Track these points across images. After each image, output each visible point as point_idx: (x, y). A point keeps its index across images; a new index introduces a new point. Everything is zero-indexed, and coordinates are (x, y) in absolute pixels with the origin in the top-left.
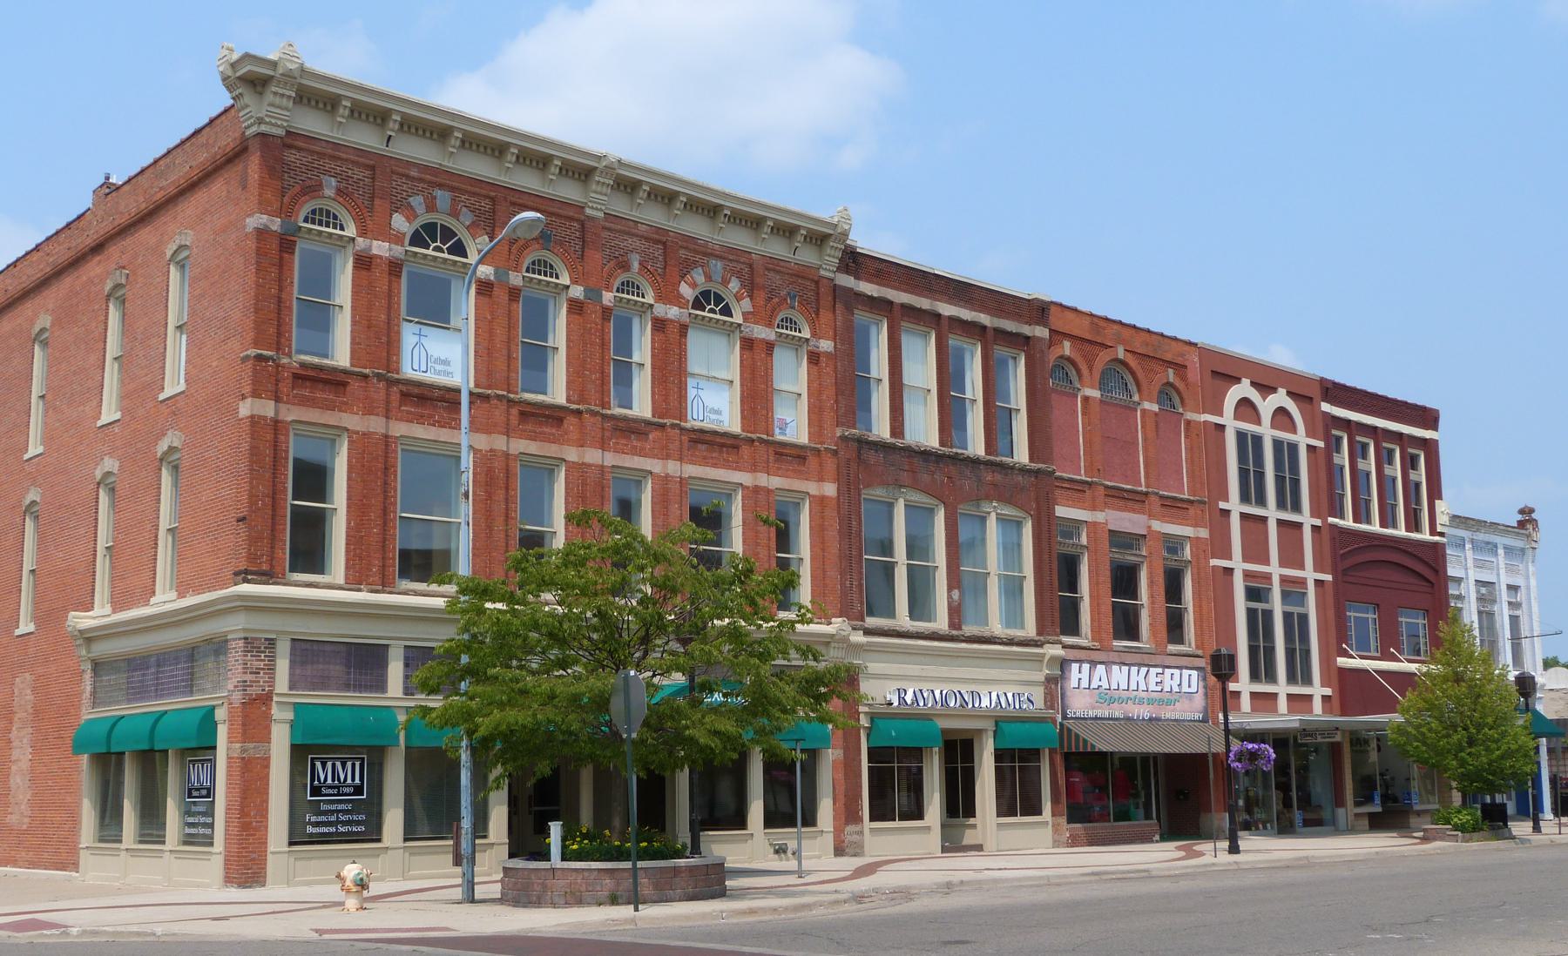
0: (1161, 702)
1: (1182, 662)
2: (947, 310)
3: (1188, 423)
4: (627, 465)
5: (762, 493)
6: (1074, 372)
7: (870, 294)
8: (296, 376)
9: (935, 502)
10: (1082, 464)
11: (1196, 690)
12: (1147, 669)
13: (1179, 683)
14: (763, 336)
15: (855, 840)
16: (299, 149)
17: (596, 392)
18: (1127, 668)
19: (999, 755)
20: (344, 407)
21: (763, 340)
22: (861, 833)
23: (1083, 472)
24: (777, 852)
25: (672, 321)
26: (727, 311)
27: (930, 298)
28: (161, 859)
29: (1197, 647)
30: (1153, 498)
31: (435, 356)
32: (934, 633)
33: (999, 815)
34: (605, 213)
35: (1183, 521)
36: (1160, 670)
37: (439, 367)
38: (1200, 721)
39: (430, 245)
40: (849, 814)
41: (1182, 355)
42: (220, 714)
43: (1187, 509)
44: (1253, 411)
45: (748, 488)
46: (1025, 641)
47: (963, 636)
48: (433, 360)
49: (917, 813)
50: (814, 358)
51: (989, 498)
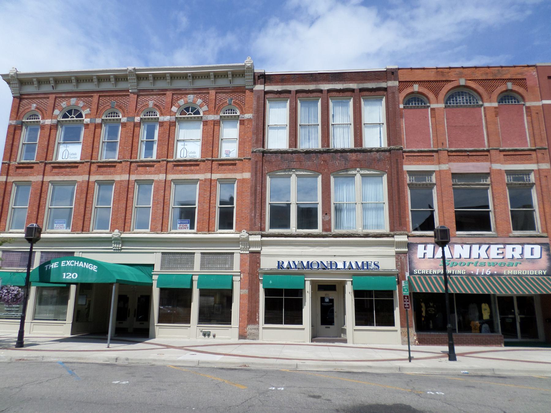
0: (503, 265)
1: (533, 240)
2: (325, 87)
3: (528, 108)
4: (142, 178)
5: (207, 181)
6: (425, 98)
7: (276, 90)
8: (18, 168)
9: (383, 173)
10: (432, 143)
11: (539, 257)
12: (487, 246)
13: (521, 253)
14: (213, 118)
15: (253, 332)
16: (26, 99)
17: (128, 154)
18: (469, 246)
19: (357, 293)
20: (31, 174)
21: (211, 121)
22: (258, 329)
23: (432, 146)
24: (204, 335)
25: (166, 122)
26: (198, 113)
27: (315, 84)
28: (329, 329)
29: (543, 231)
30: (492, 152)
31: (71, 153)
32: (309, 234)
33: (357, 324)
34: (138, 90)
35: (530, 161)
36: (502, 246)
37: (72, 156)
38: (543, 275)
39: (192, 112)
40: (252, 318)
41: (521, 74)
42: (235, 278)
43: (531, 155)
44: (52, 110)
45: (202, 180)
46: (377, 235)
47: (330, 234)
48: (189, 153)
49: (298, 320)
50: (242, 122)
51: (354, 168)
